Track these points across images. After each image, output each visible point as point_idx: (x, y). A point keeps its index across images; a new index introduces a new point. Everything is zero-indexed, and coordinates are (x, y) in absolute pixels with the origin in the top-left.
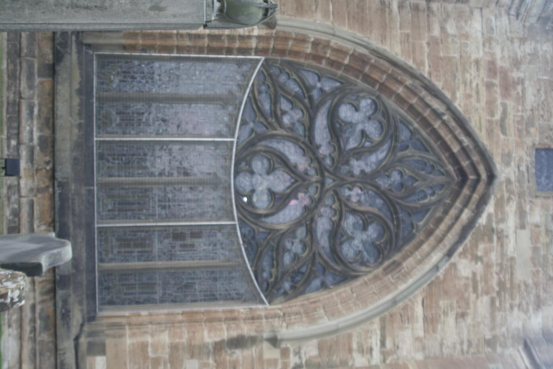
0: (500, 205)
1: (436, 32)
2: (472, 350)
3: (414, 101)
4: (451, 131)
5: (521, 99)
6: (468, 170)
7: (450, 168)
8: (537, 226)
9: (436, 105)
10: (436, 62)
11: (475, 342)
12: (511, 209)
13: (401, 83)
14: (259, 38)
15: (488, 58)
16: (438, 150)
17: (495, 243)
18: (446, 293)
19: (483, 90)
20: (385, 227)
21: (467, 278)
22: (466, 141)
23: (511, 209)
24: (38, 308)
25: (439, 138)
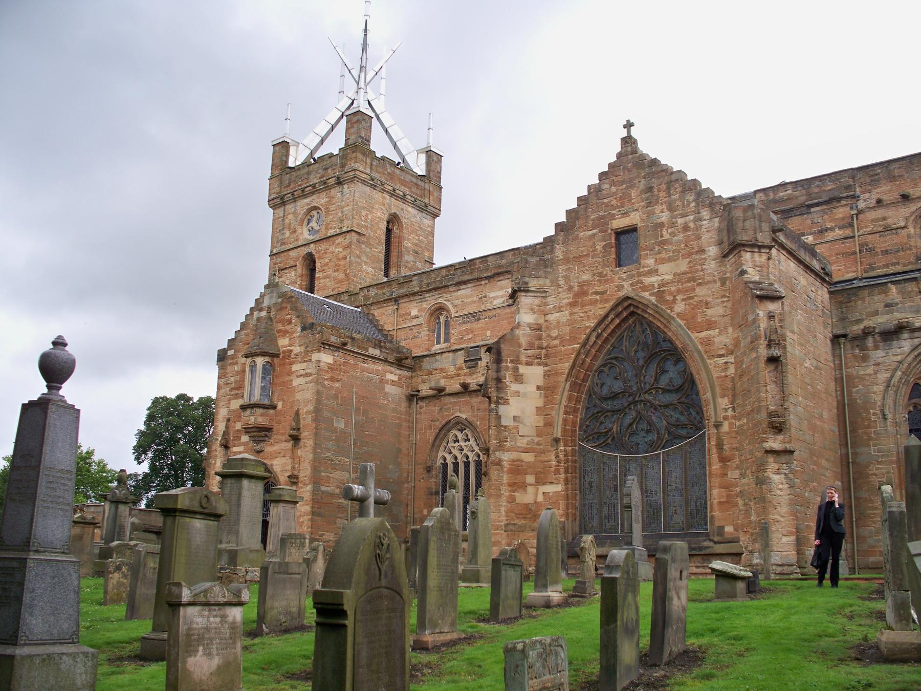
0: (644, 289)
1: (557, 342)
2: (727, 294)
3: (593, 351)
4: (607, 326)
5: (588, 283)
6: (629, 311)
7: (630, 322)
8: (656, 261)
9: (593, 339)
10: (572, 340)
11: (723, 293)
12: (647, 280)
13: (584, 361)
14: (566, 445)
15: (568, 307)
16: (622, 330)
17: (666, 289)
18: (693, 317)
19: (585, 309)
20: (665, 359)
21: (685, 304)
22: (611, 316)
23: (647, 280)
24: (698, 564)
25: (613, 331)
